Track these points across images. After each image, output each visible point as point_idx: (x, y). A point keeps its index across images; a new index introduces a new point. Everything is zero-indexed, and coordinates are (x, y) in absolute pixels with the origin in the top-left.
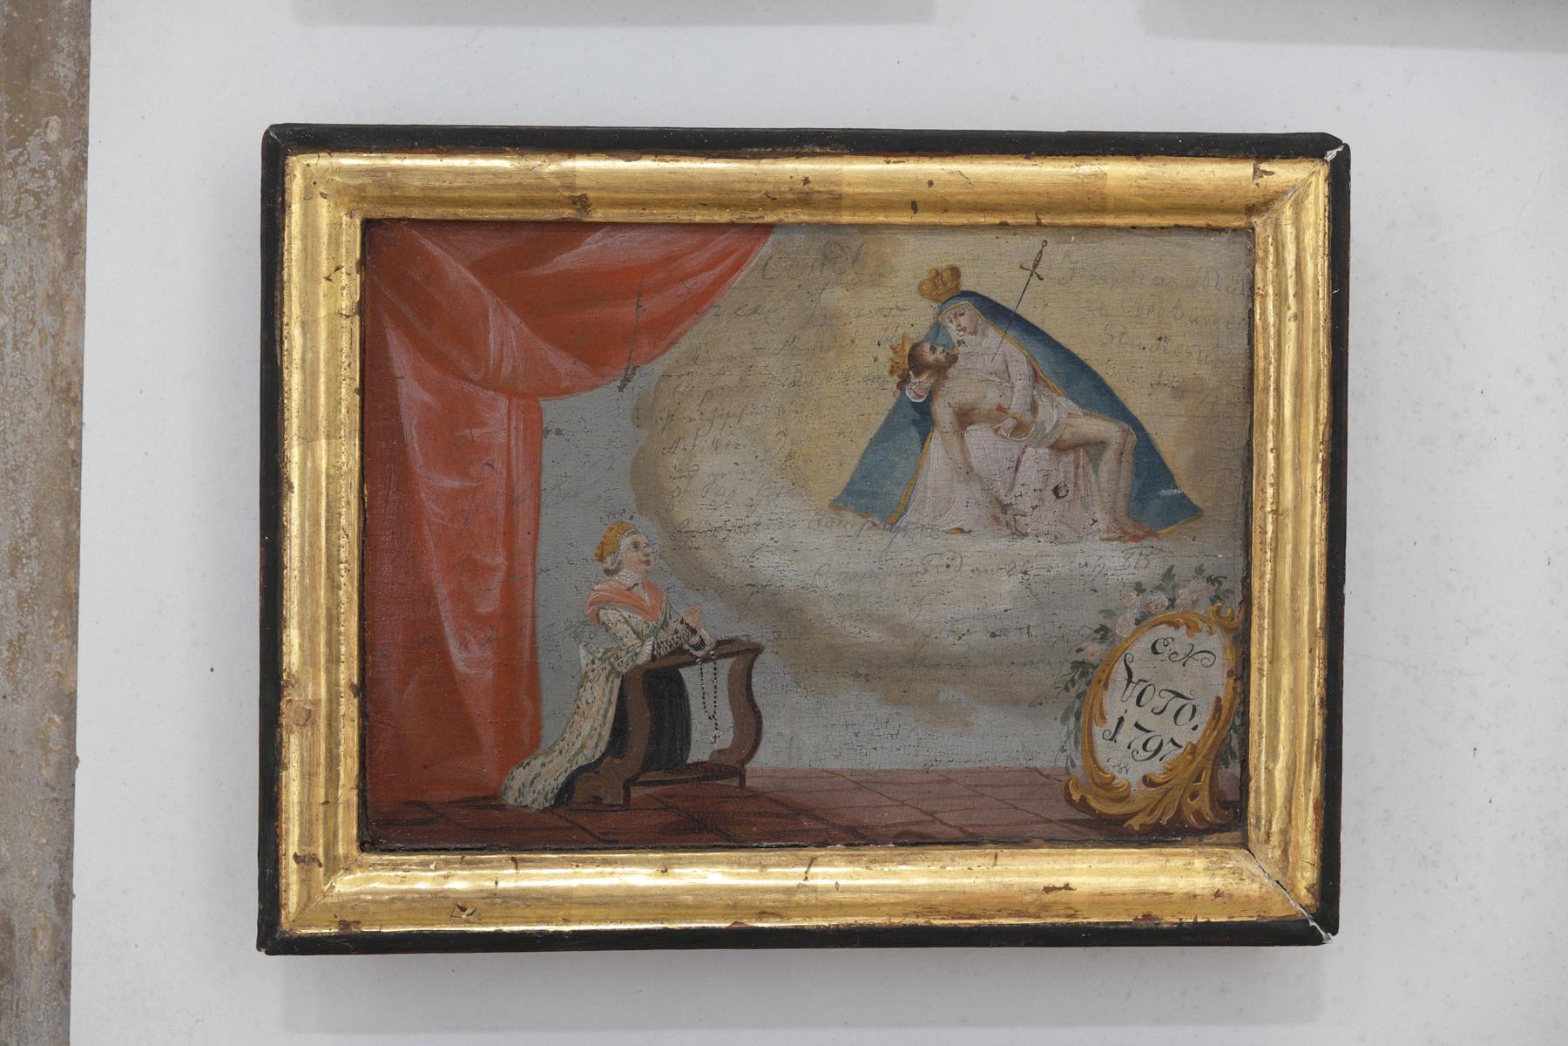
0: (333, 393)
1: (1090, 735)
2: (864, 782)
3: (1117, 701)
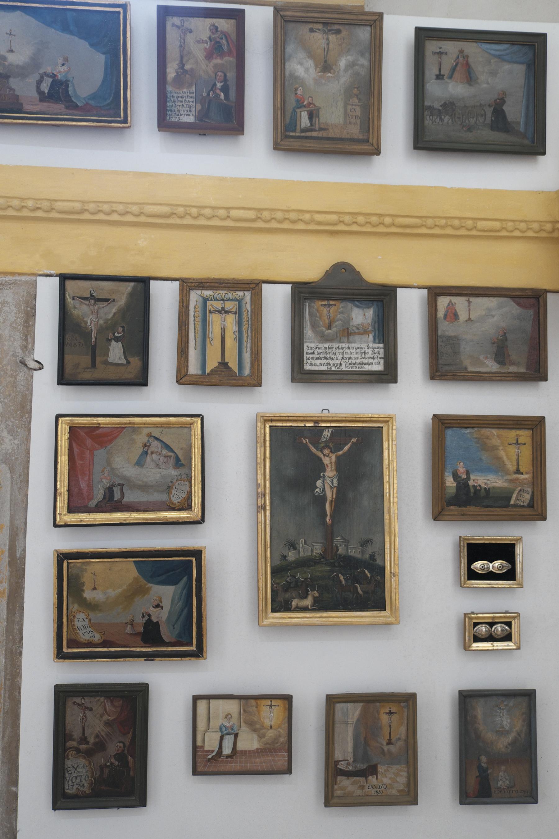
0: (65, 450)
1: (170, 496)
2: (139, 503)
3: (174, 491)
